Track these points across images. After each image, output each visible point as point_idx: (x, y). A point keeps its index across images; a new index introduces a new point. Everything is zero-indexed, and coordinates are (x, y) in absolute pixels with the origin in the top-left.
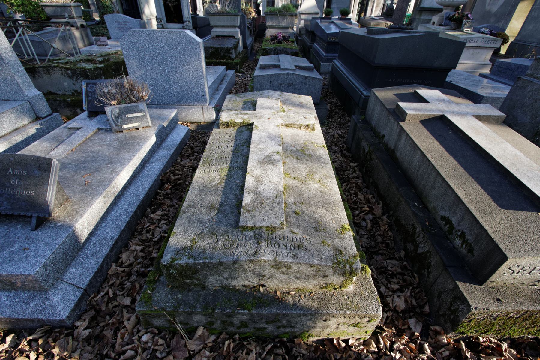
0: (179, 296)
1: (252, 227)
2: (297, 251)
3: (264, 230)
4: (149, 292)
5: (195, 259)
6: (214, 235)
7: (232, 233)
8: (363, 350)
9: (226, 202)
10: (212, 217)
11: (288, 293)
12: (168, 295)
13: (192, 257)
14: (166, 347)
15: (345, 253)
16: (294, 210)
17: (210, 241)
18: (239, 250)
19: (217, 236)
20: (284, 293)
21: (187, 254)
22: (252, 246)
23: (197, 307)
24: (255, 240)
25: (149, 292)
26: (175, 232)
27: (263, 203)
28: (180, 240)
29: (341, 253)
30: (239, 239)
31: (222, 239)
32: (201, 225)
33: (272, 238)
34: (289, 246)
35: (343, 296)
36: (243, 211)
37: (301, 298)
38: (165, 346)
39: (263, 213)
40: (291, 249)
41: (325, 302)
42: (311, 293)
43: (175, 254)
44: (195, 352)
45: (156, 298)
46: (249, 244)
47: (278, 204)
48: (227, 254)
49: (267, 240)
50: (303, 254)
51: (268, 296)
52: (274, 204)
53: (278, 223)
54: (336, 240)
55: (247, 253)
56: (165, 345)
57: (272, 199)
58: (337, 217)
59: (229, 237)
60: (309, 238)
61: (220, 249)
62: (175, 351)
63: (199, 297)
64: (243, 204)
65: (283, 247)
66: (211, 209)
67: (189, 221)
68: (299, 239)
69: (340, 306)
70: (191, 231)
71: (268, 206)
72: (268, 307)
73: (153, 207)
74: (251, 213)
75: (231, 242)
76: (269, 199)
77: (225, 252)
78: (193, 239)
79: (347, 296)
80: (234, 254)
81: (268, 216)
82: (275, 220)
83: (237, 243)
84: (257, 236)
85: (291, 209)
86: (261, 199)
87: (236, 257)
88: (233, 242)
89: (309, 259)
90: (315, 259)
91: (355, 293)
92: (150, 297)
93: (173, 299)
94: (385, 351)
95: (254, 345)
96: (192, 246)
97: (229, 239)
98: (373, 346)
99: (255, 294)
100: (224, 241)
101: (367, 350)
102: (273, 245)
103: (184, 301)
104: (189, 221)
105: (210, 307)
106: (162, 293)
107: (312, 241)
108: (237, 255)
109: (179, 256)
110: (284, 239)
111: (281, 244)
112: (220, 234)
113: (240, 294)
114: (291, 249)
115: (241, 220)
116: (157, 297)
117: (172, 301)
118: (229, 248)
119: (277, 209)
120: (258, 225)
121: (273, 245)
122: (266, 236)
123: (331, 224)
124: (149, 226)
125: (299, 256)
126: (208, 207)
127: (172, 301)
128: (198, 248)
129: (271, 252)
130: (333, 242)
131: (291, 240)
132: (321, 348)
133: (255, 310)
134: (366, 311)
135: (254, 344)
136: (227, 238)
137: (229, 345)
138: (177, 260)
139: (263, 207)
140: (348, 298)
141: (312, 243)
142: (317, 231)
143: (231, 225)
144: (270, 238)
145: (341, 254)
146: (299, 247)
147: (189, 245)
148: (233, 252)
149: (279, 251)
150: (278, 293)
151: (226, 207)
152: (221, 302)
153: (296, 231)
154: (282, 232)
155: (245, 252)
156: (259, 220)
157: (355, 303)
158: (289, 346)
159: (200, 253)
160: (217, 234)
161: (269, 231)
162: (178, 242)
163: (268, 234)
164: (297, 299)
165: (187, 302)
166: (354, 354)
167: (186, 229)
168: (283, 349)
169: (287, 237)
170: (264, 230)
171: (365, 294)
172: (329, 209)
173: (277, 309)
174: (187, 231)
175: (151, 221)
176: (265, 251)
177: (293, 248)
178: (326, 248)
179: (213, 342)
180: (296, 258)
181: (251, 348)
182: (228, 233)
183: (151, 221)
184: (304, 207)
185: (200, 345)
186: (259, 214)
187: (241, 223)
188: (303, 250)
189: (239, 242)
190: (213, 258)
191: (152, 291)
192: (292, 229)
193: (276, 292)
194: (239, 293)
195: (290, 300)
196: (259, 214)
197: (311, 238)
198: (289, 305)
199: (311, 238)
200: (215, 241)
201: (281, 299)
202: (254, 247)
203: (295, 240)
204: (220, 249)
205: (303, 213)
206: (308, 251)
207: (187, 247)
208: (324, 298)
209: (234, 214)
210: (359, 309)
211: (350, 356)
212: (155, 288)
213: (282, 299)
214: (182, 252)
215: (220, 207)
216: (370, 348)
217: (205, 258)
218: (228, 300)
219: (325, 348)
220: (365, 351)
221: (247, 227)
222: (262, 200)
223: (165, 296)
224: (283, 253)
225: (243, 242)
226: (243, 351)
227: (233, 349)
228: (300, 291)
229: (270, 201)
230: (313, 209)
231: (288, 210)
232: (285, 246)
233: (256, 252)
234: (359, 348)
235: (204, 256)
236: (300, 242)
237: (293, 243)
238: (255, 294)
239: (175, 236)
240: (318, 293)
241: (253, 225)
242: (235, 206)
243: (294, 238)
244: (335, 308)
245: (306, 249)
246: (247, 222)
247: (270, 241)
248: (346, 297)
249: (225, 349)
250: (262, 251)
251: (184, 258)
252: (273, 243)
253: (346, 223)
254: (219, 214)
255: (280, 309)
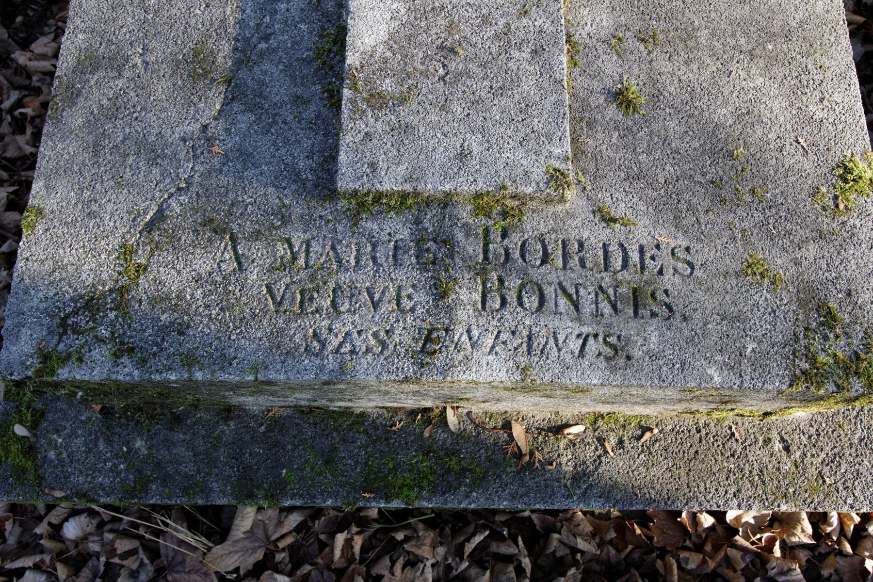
0: (139, 443)
1: (404, 196)
2: (627, 327)
3: (465, 213)
4: (20, 430)
5: (144, 361)
6: (219, 231)
7: (307, 222)
8: (771, 541)
9: (266, 38)
10: (205, 127)
11: (558, 430)
12: (96, 441)
13: (131, 350)
14: (146, 561)
15: (847, 318)
16: (609, 83)
17: (203, 264)
18: (345, 324)
19: (233, 239)
20: (540, 430)
21: (104, 332)
22: (407, 304)
23: (211, 490)
24: (423, 267)
25: (20, 430)
26: (40, 212)
27: (452, 50)
28: (68, 256)
29: (829, 318)
30: (339, 262)
31: (256, 251)
32: (156, 171)
33: (507, 255)
34: (587, 297)
35: (767, 441)
36: (353, 102)
37: (606, 452)
38: (142, 554)
39: (458, 109)
40: (598, 314)
41: (697, 466)
42: (645, 429)
43: (51, 333)
44: (242, 572)
45: (52, 454)
46: (392, 292)
47: (535, 52)
48: (287, 344)
49: (482, 272)
50: (654, 339)
51: (478, 443)
52: (515, 53)
53: (538, 173)
54: (811, 251)
55: (384, 345)
56: (141, 552)
57: (502, 22)
58: (819, 115)
59: (288, 241)
60: (685, 244)
61: (254, 316)
62: (178, 572)
63: (215, 447)
64: (352, 59)
65: (563, 302)
66: (194, 77)
67: (96, 149)
68: (635, 257)
69: (752, 482)
70: (110, 207)
71: (483, 66)
72: (479, 486)
73: (19, 19)
74: (393, 111)
75: (303, 275)
76: (486, 21)
77: (281, 332)
78: (126, 252)
79: (782, 440)
80: (323, 345)
81: (483, 131)
82: (520, 153)
83: (331, 285)
84: (431, 245)
85: (597, 75)
86: (442, 22)
87: (331, 363)
88: (312, 278)
89: (683, 365)
90: (710, 361)
91: (813, 431)
92: (29, 449)
93: (117, 456)
94: (839, 542)
95: (428, 541)
96: (122, 291)
97: (294, 258)
98: (803, 531)
99: (426, 434)
100: (272, 269)
101: (784, 546)
102: (512, 297)
103: (158, 465)
104: (96, 145)
105: (258, 487)
106: (73, 434)
107: (697, 260)
108: (337, 351)
109: (73, 341)
110: (566, 256)
111: (549, 291)
112: (249, 228)
113: (370, 436)
114: (598, 314)
115: (342, 157)
116: (56, 447)
117: (116, 466)
118: (296, 309)
119: (528, 87)
120: (431, 186)
121: (512, 297)
122: (473, 248)
123: (792, 158)
124: (19, 104)
125: (637, 353)
126: (178, 64)
127: (116, 466)
128: (154, 301)
129: (504, 336)
130: (797, 263)
131: (596, 264)
132: (638, 531)
133: (429, 500)
134: (850, 501)
135: (428, 536)
136: (281, 249)
137: (349, 543)
138: (65, 359)
139: (459, 76)
140: (787, 449)
141: (698, 273)
142: (723, 201)
143: (297, 178)
144: (497, 256)
145: (831, 328)
146: (637, 298)
147: (110, 285)
148: (315, 335)
149: (547, 322)
150: (518, 431)
151: (266, 66)
152: (301, 469)
153: (620, 210)
154: (555, 215)
155: (375, 335)
156: (440, 156)
157: (812, 471)
158: (536, 521)
159: (164, 330)
160: (235, 227)
161: (488, 216)
162: (59, 266)
163: (487, 231)
164: (589, 453)
165: (170, 469)
166: (743, 558)
167: (87, 194)
168: (521, 542)
169: (581, 245)
170: (465, 213)
171: (853, 433)
172: (779, 71)
173: (513, 497)
174: (95, 207)
175: (21, 80)
176: (475, 333)
177: (607, 309)
178: (762, 296)
179: (297, 530)
180: (622, 361)
181: (418, 552)
182: (286, 220)
183: (21, 80)
184: (663, 65)
185: (254, 550)
186: (434, 118)
187: (345, 182)
188: (654, 315)
189: (344, 278)
190: (225, 361)
191: (33, 427)
192: (604, 197)
193: (507, 426)
194: (366, 432)
195: (564, 460)
196: (434, 118)
197: (696, 246)
198: (558, 480)
199: (696, 246)
200: (230, 266)
201: (527, 458)
202: (419, 311)
203: (618, 264)
204: (254, 316)
205: (656, 97)
206: (677, 321)
207: (103, 295)
208: (692, 451)
209: (310, 112)
210: (827, 495)
211: (728, 561)
212: (43, 414)
213: (531, 454)
214: (82, 320)
215: (239, 64)
216: (794, 535)
217: (190, 361)
218: (327, 462)
219: (648, 528)
220: (777, 551)
221: (379, 197)
222: (451, 27)
223: (85, 444)
224: (561, 340)
225: (363, 280)
226: (393, 562)
227: (363, 550)
228: (600, 423)
229: (490, 32)
230: (707, 74)
231: (584, 81)
232: (569, 296)
233: (428, 339)
234: (758, 536)
235: (184, 349)
236: (643, 268)
237: (607, 279)
238: (426, 434)
239: (40, 228)
240: (670, 427)
241: (408, 188)
242: (308, 62)
243: (614, 248)
244: (734, 489)
245: (669, 307)
246: (373, 166)
247: (494, 276)
248: (778, 446)
249: (338, 553)
250: (459, 331)
251: (96, 353)
252: (513, 283)
253: (859, 149)
254: (236, 106)
255: (526, 494)
